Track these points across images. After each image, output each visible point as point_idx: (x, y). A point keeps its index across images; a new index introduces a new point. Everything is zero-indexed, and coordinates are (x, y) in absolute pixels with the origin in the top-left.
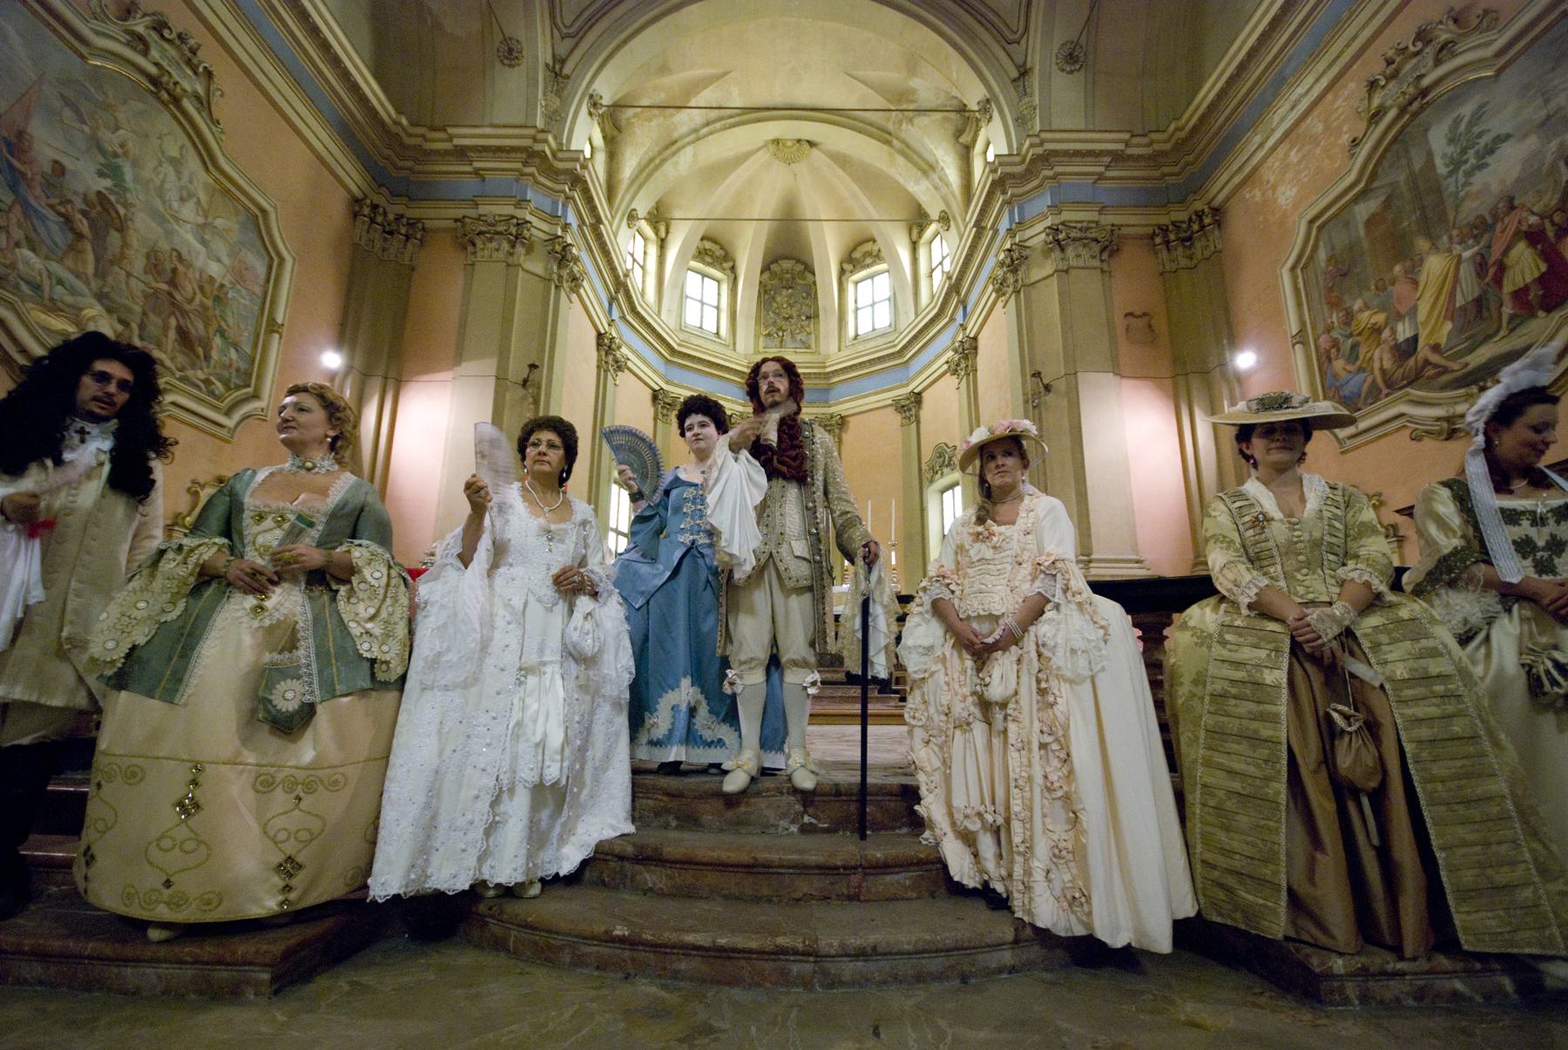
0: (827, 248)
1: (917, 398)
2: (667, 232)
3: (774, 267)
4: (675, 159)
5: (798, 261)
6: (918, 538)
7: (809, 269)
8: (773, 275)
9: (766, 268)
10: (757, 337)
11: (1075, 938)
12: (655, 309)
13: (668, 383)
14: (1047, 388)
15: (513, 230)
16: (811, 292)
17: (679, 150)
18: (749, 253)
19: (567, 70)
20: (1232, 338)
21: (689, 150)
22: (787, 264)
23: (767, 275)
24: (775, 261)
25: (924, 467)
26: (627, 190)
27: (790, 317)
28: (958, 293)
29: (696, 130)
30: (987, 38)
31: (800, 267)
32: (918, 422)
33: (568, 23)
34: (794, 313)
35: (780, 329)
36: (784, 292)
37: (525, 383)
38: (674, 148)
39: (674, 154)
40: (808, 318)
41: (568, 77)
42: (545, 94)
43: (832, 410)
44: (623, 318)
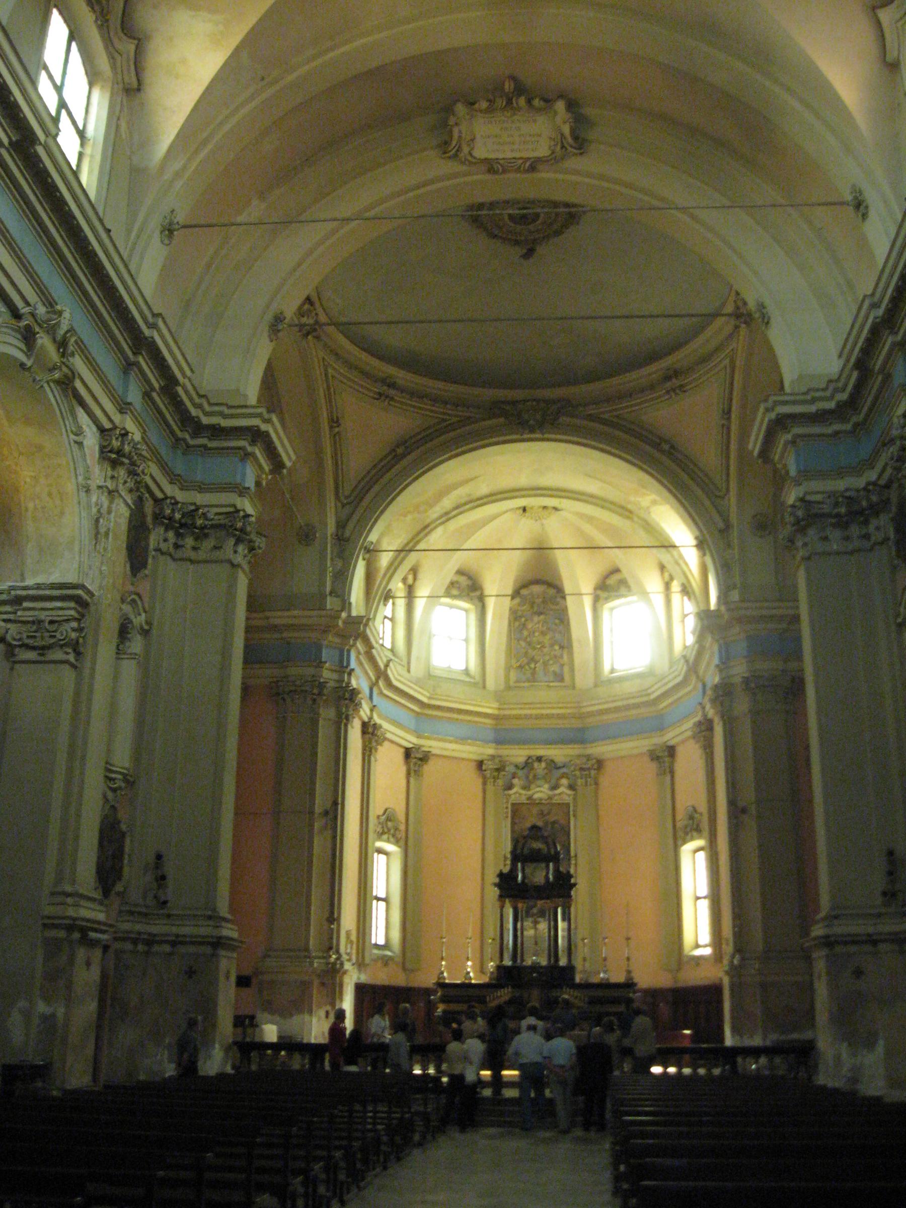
0: (578, 576)
1: (671, 751)
2: (415, 579)
3: (524, 592)
4: (427, 538)
5: (550, 585)
6: (672, 867)
7: (559, 591)
8: (524, 599)
9: (516, 594)
10: (508, 669)
11: (467, 986)
12: (405, 662)
13: (419, 737)
14: (744, 811)
15: (315, 691)
16: (562, 618)
17: (429, 533)
18: (498, 580)
19: (347, 533)
20: (611, 1071)
21: (440, 530)
22: (537, 589)
23: (517, 600)
24: (525, 586)
25: (679, 825)
26: (385, 575)
27: (543, 647)
28: (696, 672)
29: (446, 513)
30: (699, 492)
31: (552, 591)
32: (672, 777)
33: (347, 493)
34: (546, 640)
35: (533, 660)
36: (536, 619)
37: (326, 813)
38: (427, 530)
39: (426, 535)
40: (562, 647)
41: (348, 540)
42: (332, 559)
43: (589, 751)
44: (381, 693)
